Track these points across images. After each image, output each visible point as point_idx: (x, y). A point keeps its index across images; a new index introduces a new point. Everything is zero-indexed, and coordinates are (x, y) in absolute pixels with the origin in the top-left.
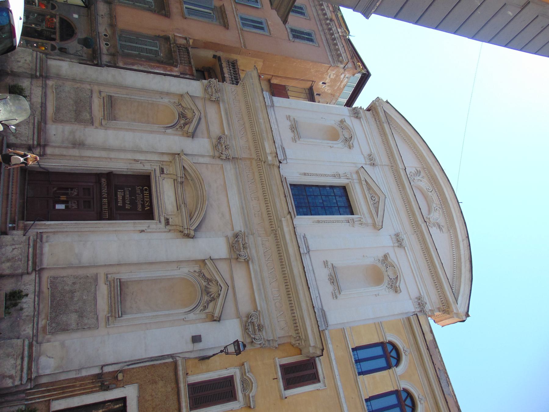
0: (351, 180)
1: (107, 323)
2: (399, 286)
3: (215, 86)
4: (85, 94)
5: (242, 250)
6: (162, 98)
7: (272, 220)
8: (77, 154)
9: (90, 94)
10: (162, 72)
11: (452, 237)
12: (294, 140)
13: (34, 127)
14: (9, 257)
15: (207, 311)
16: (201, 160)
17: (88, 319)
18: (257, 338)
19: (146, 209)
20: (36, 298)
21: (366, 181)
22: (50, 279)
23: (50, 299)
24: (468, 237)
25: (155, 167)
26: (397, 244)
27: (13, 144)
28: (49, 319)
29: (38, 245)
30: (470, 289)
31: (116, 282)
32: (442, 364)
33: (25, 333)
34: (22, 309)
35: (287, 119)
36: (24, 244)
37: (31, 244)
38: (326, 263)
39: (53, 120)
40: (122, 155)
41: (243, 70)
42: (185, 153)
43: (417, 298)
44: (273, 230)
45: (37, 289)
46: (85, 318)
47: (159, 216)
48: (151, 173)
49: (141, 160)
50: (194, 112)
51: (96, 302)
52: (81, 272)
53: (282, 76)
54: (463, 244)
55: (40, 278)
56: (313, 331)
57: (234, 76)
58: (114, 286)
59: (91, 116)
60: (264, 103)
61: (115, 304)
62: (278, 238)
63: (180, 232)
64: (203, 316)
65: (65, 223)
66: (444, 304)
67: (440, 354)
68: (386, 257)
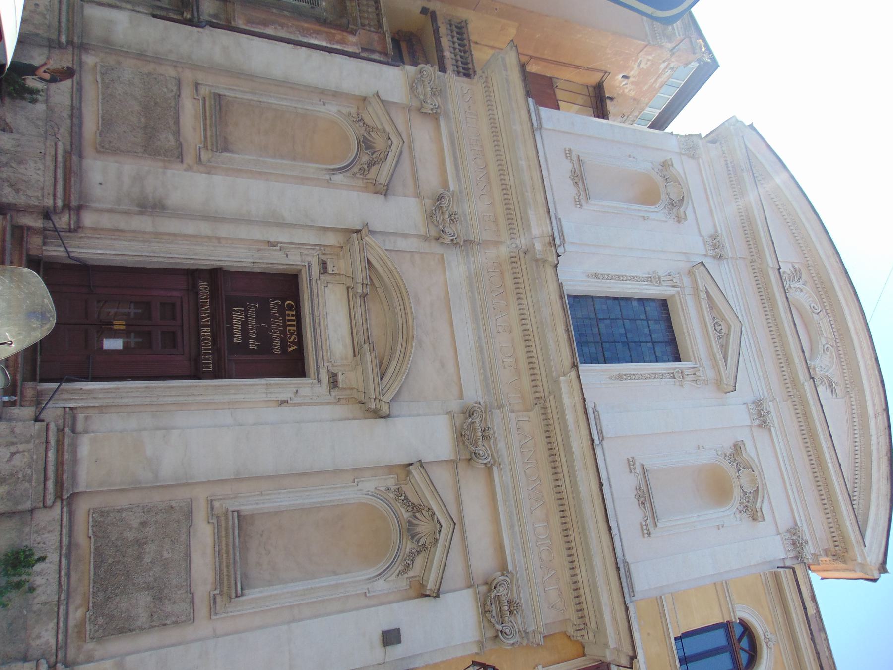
0: (679, 289)
1: (213, 610)
2: (761, 508)
3: (430, 81)
4: (165, 90)
5: (480, 443)
6: (324, 104)
7: (538, 377)
8: (149, 228)
9: (175, 89)
10: (324, 44)
11: (854, 407)
12: (578, 203)
13: (56, 167)
15: (411, 573)
16: (402, 244)
17: (174, 603)
18: (507, 631)
19: (290, 350)
20: (64, 561)
21: (707, 292)
22: (93, 517)
23: (92, 561)
24: (886, 410)
25: (309, 259)
26: (757, 422)
27: (9, 205)
28: (91, 608)
29: (67, 441)
30: (887, 516)
31: (230, 518)
32: (831, 663)
33: (38, 642)
34: (32, 589)
35: (566, 157)
36: (37, 441)
37: (52, 442)
38: (631, 463)
39: (96, 149)
40: (243, 232)
41: (476, 43)
42: (371, 229)
43: (788, 531)
44: (538, 398)
45: (65, 541)
46: (167, 602)
47: (317, 368)
48: (300, 271)
49: (281, 243)
50: (390, 139)
51: (190, 564)
52: (156, 498)
53: (549, 58)
54: (876, 423)
55: (71, 514)
56: (614, 618)
57: (461, 57)
58: (227, 529)
59: (177, 140)
60: (529, 124)
61: (228, 566)
62: (549, 416)
63: (360, 402)
64: (403, 583)
65: (125, 388)
66: (837, 544)
67: (828, 643)
68: (738, 447)
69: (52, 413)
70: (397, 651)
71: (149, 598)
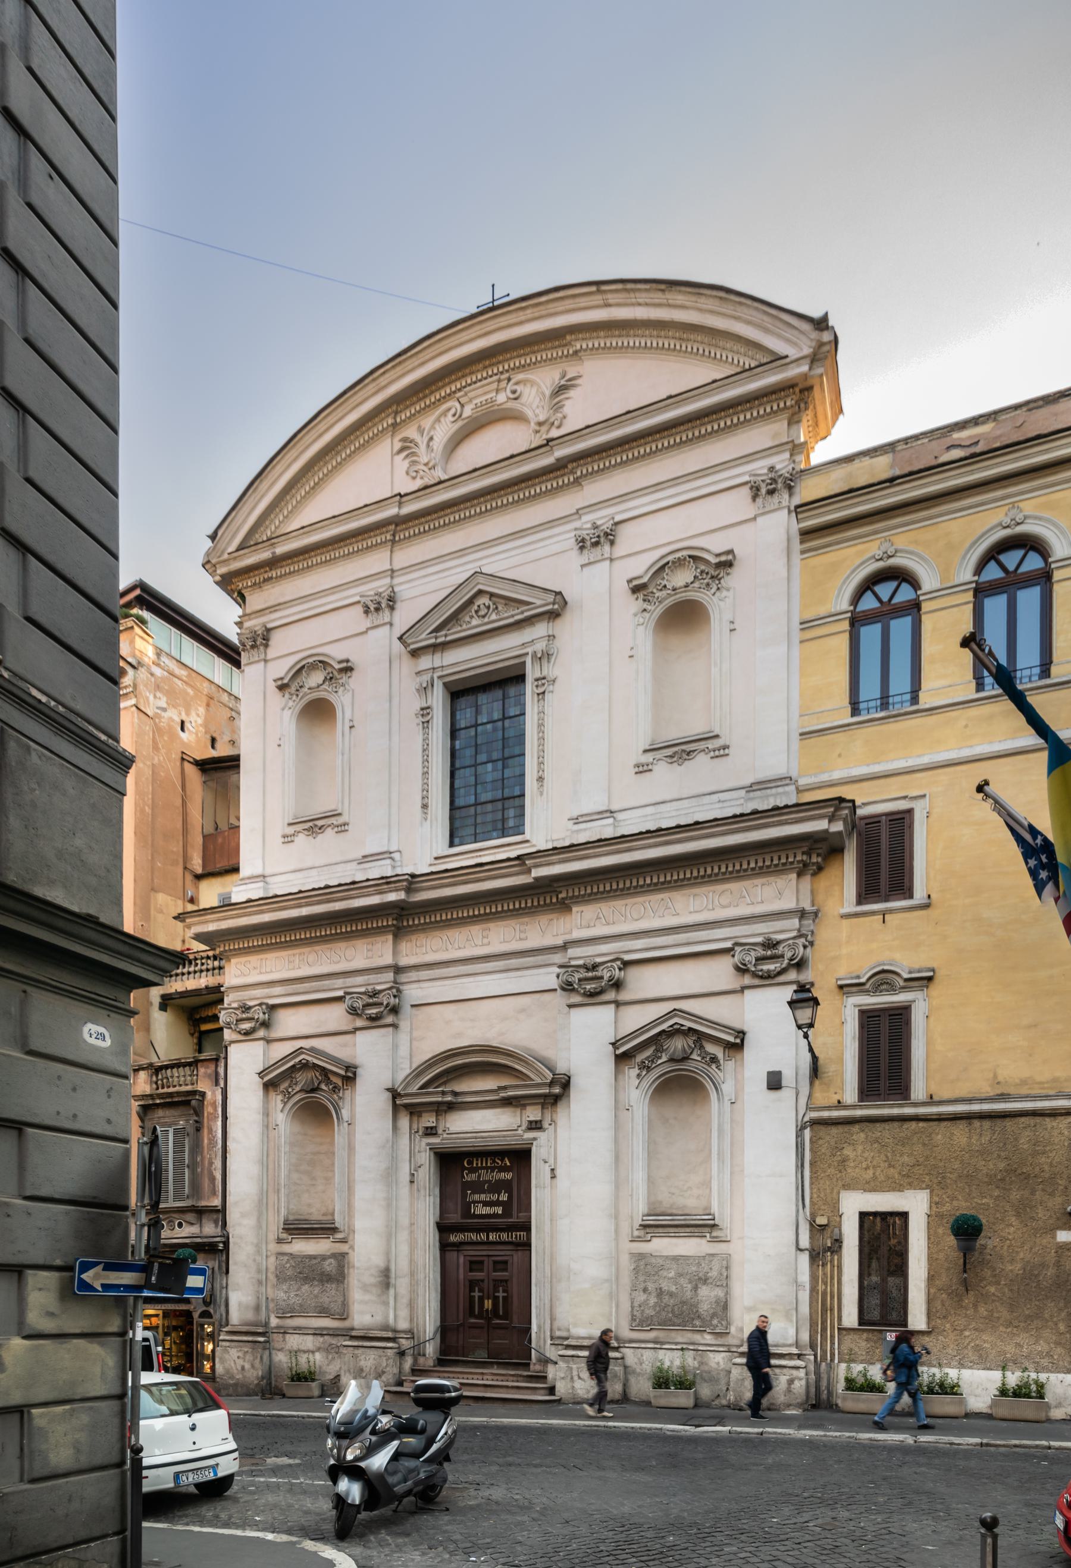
9: (286, 1258)
10: (219, 1123)
19: (508, 1164)
33: (722, 1363)
46: (710, 1274)
52: (626, 1280)
55: (631, 1341)
67: (911, 437)
69: (551, 1353)
70: (788, 1078)
71: (704, 1287)
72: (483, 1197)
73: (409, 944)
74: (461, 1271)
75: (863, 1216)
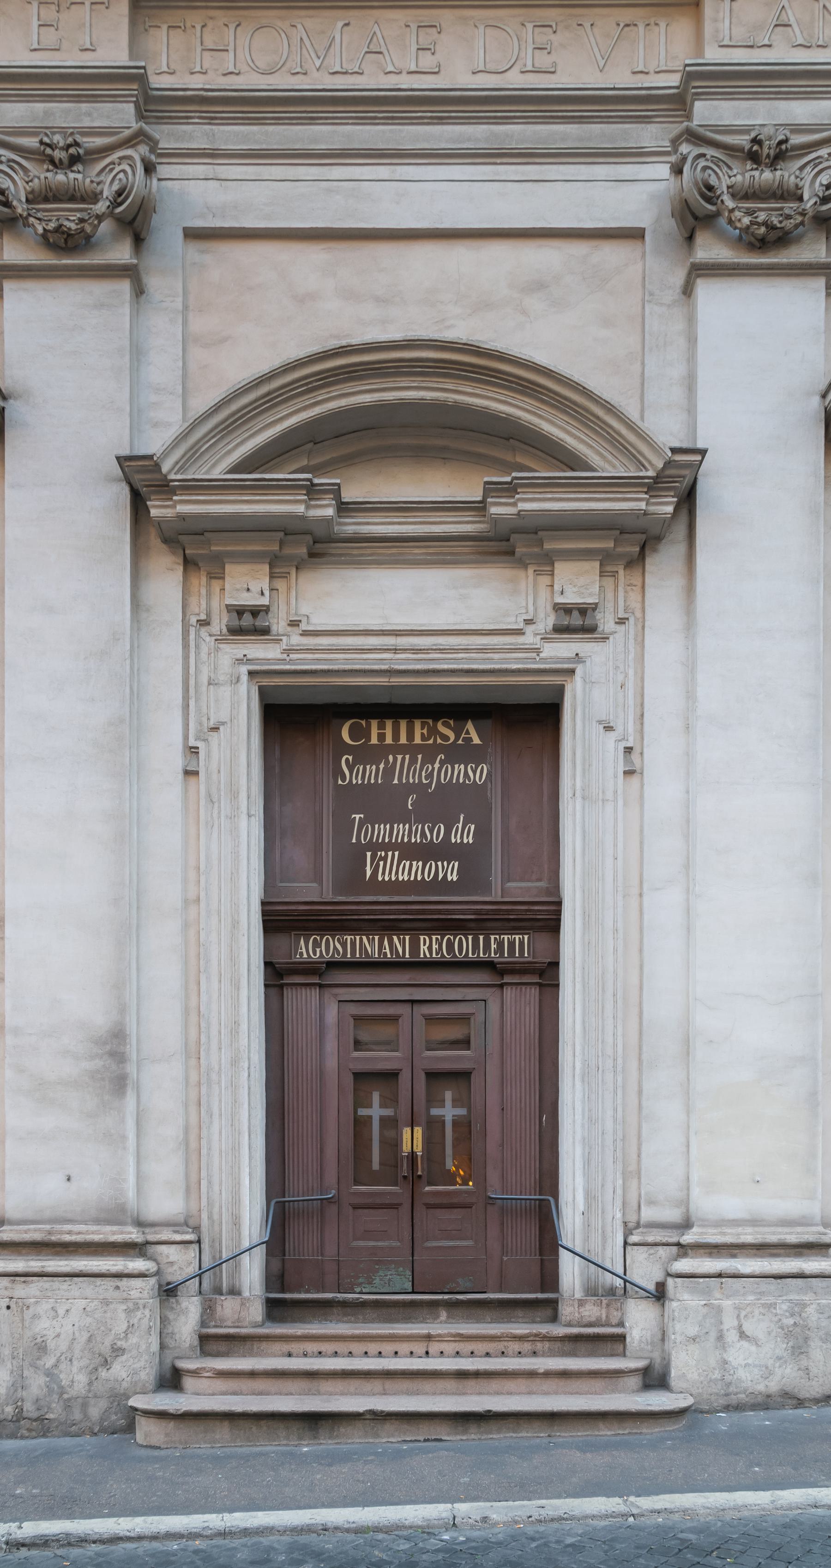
14: (779, 1352)
19: (476, 740)
36: (717, 1295)
49: (186, 737)
72: (401, 831)
73: (177, 37)
74: (331, 1045)
75: (371, 1107)
